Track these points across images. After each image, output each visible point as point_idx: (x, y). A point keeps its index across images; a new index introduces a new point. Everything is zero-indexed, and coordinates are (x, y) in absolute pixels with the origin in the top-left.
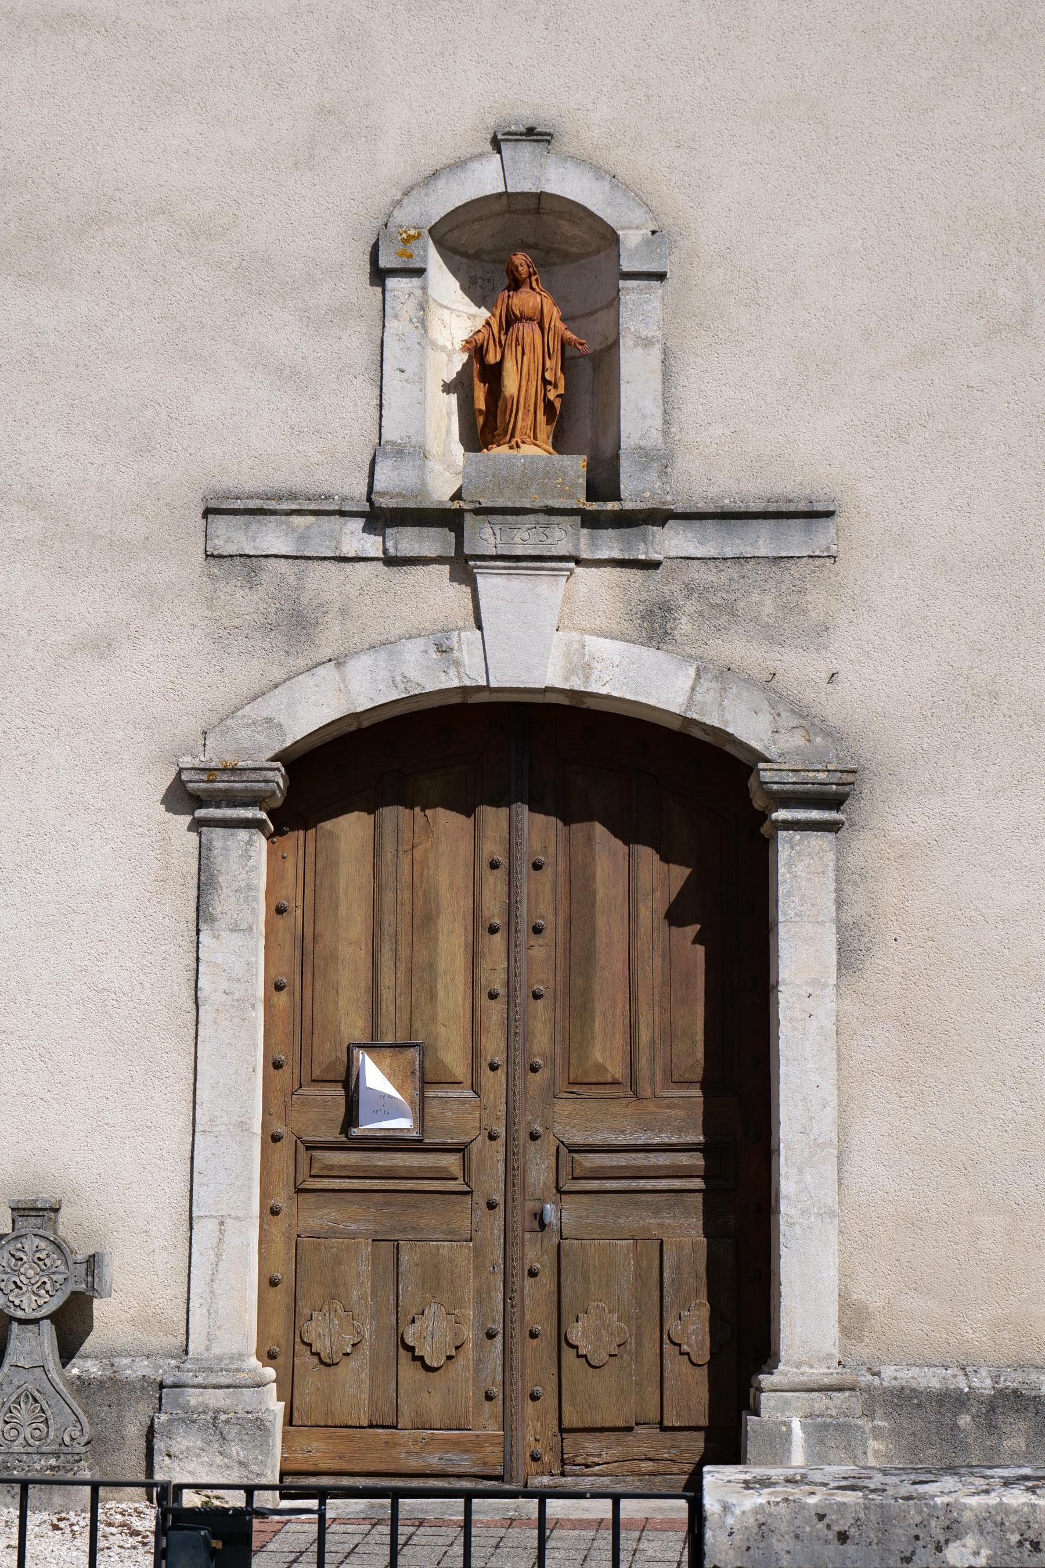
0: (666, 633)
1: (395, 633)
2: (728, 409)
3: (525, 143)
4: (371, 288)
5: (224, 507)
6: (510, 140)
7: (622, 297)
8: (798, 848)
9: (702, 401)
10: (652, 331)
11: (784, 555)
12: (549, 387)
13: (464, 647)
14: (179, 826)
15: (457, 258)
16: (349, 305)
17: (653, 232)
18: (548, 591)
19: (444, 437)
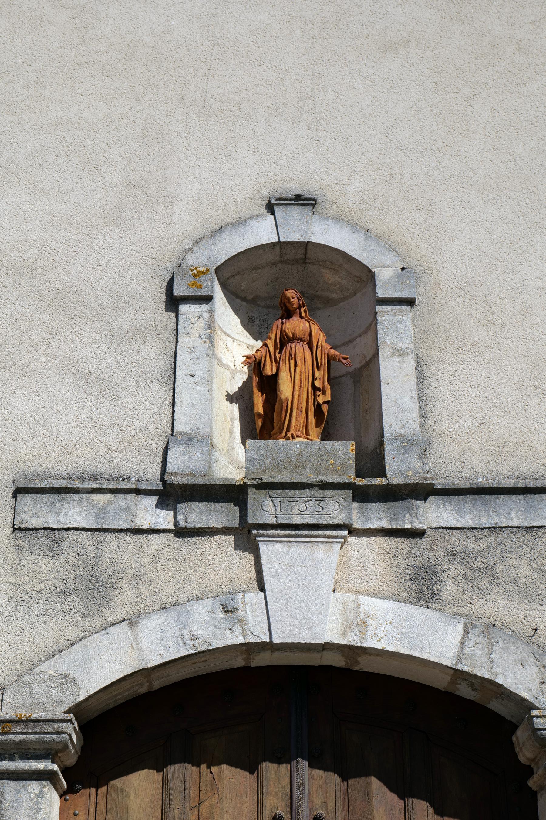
1: (184, 596)
2: (475, 405)
3: (294, 207)
4: (166, 313)
5: (32, 486)
6: (282, 204)
7: (379, 318)
9: (452, 399)
10: (406, 344)
11: (535, 524)
12: (318, 393)
13: (248, 607)
15: (238, 300)
16: (147, 326)
17: (403, 269)
18: (325, 556)
19: (227, 436)
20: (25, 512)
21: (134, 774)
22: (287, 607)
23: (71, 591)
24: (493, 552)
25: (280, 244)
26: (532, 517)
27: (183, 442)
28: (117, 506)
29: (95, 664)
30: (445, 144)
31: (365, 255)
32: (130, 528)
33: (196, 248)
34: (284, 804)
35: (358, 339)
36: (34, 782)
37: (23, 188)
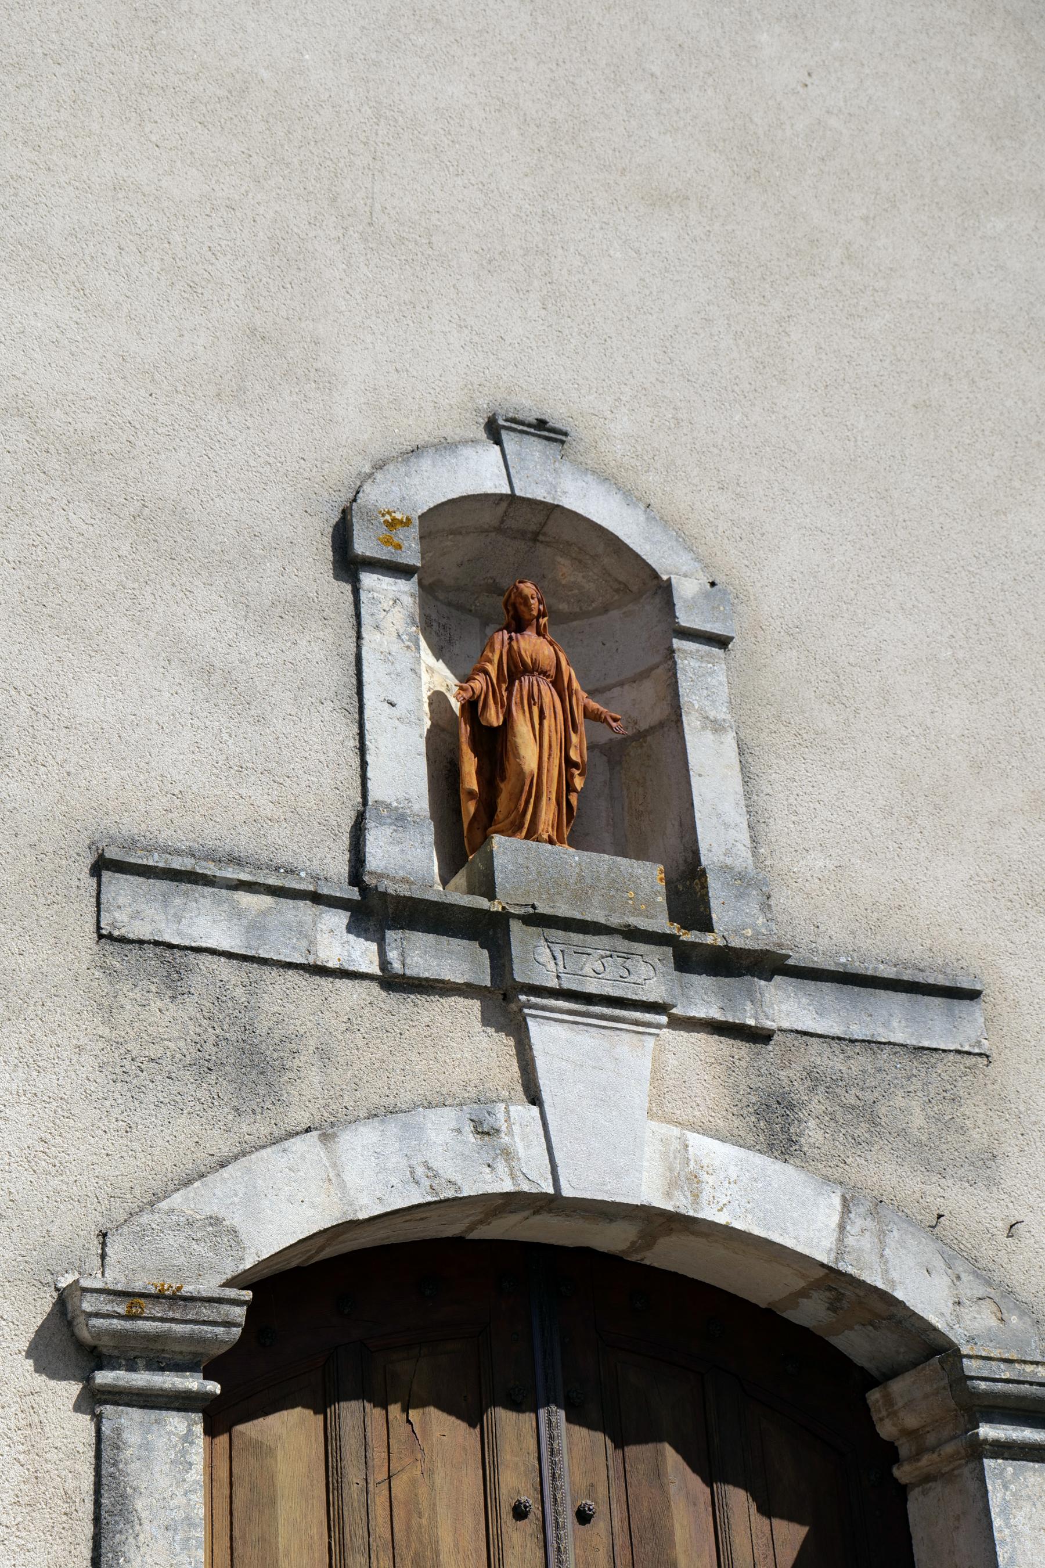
0: (790, 1140)
1: (405, 1098)
3: (533, 438)
4: (336, 583)
5: (132, 860)
6: (514, 430)
8: (1012, 1487)
9: (794, 818)
10: (721, 713)
11: (926, 1044)
13: (516, 1128)
14: (59, 1403)
16: (305, 600)
20: (119, 907)
21: (277, 1415)
22: (580, 1135)
23: (210, 1065)
24: (871, 1082)
25: (512, 499)
26: (921, 1031)
27: (389, 821)
28: (281, 919)
29: (267, 1203)
30: (753, 388)
33: (379, 476)
34: (529, 1486)
35: (616, 691)
36: (174, 1413)
37: (65, 293)
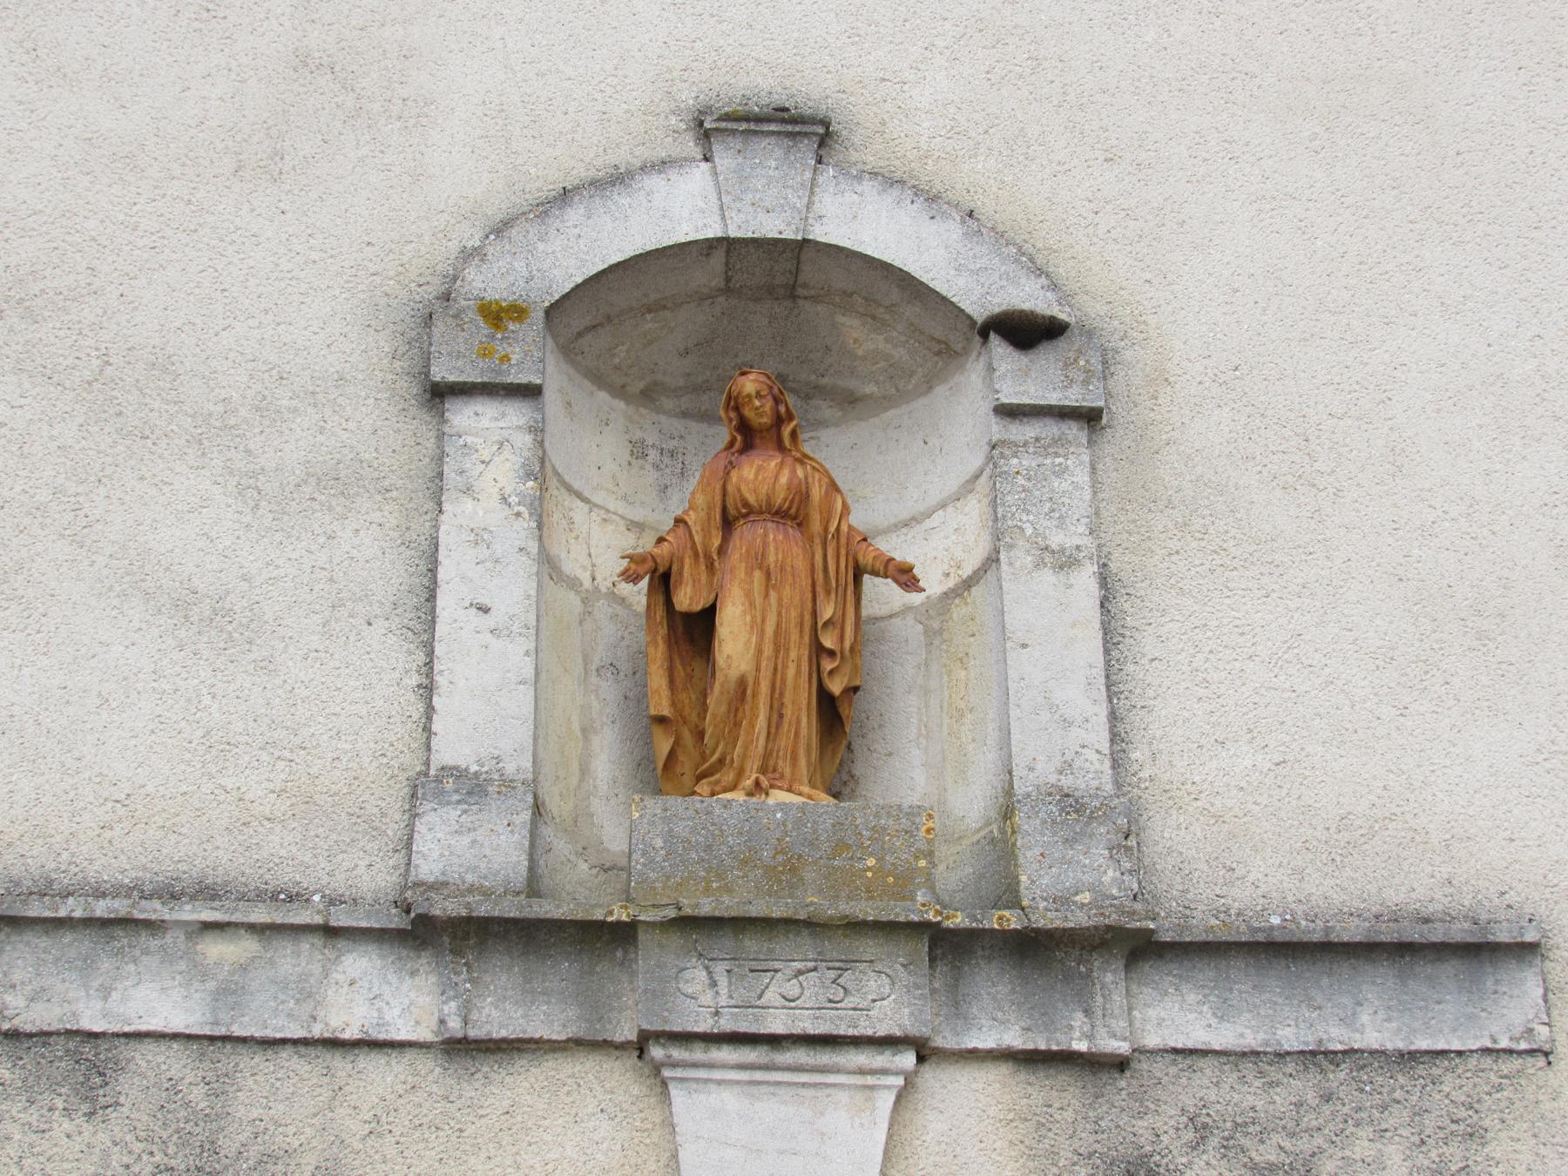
6: (733, 132)
9: (1201, 692)
10: (1073, 536)
11: (1423, 1044)
19: (574, 781)
20: (13, 986)
24: (1309, 1120)
25: (728, 245)
26: (1416, 1025)
27: (456, 797)
28: (271, 973)
31: (961, 282)
32: (309, 1036)
